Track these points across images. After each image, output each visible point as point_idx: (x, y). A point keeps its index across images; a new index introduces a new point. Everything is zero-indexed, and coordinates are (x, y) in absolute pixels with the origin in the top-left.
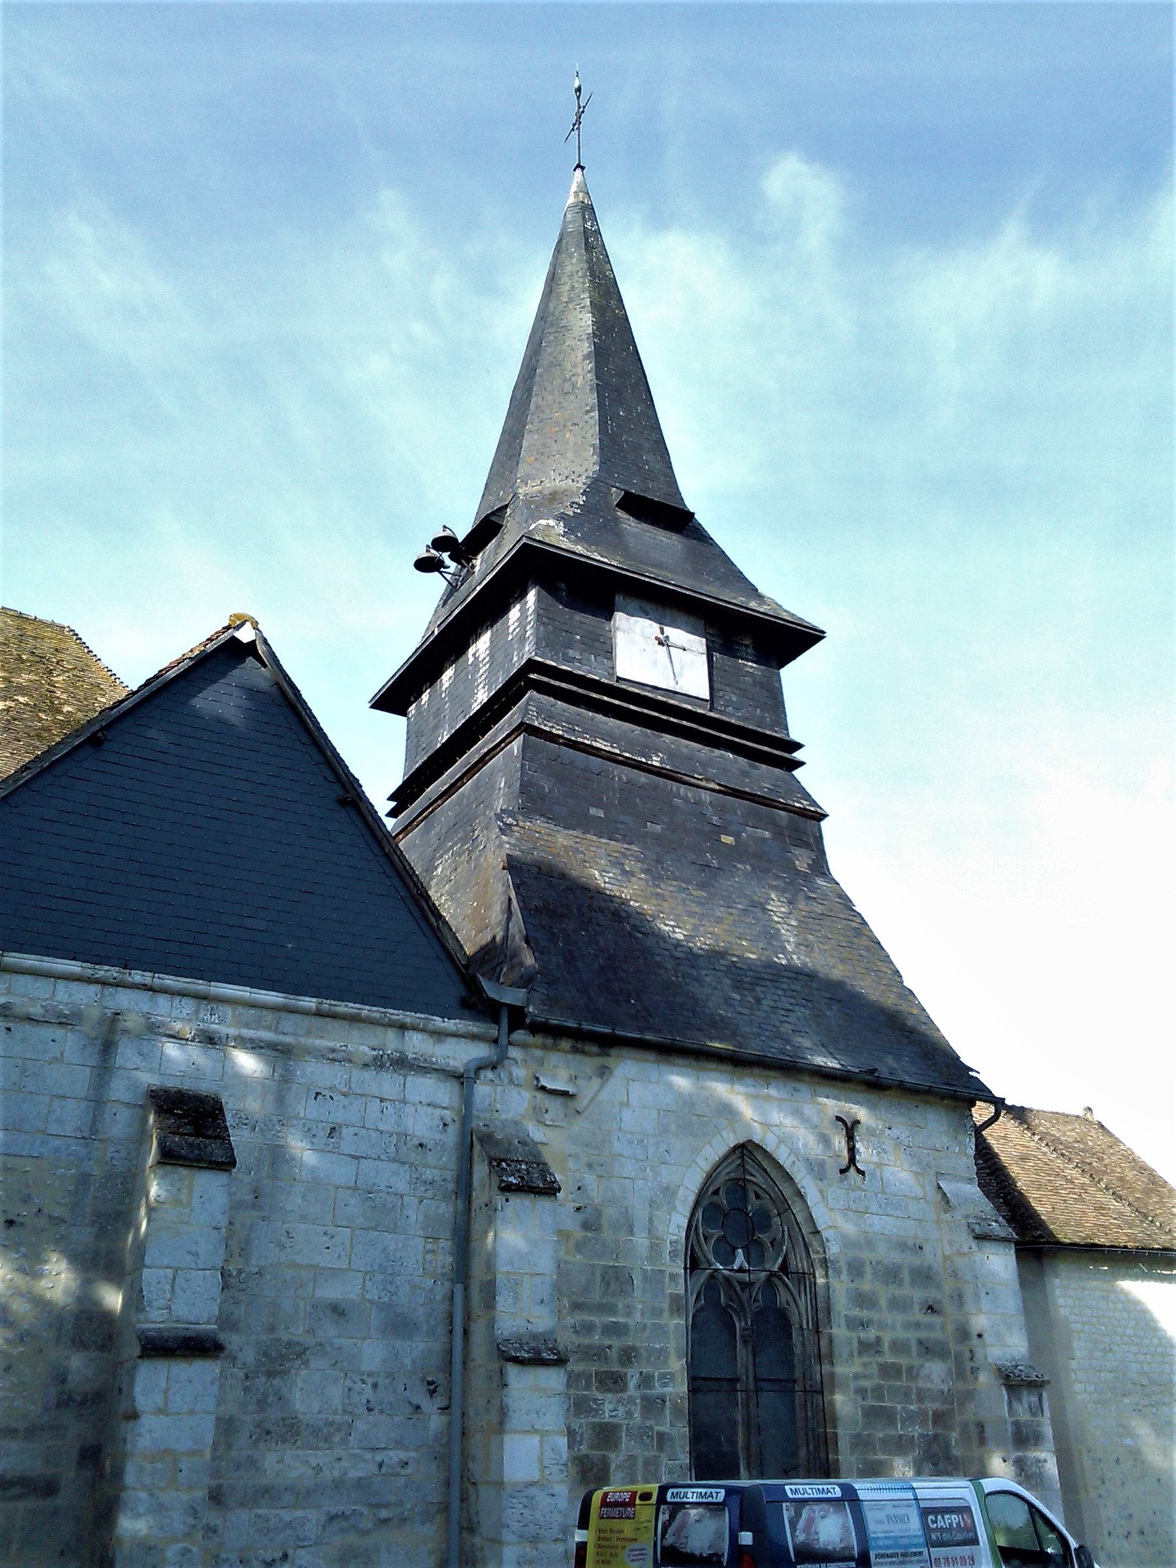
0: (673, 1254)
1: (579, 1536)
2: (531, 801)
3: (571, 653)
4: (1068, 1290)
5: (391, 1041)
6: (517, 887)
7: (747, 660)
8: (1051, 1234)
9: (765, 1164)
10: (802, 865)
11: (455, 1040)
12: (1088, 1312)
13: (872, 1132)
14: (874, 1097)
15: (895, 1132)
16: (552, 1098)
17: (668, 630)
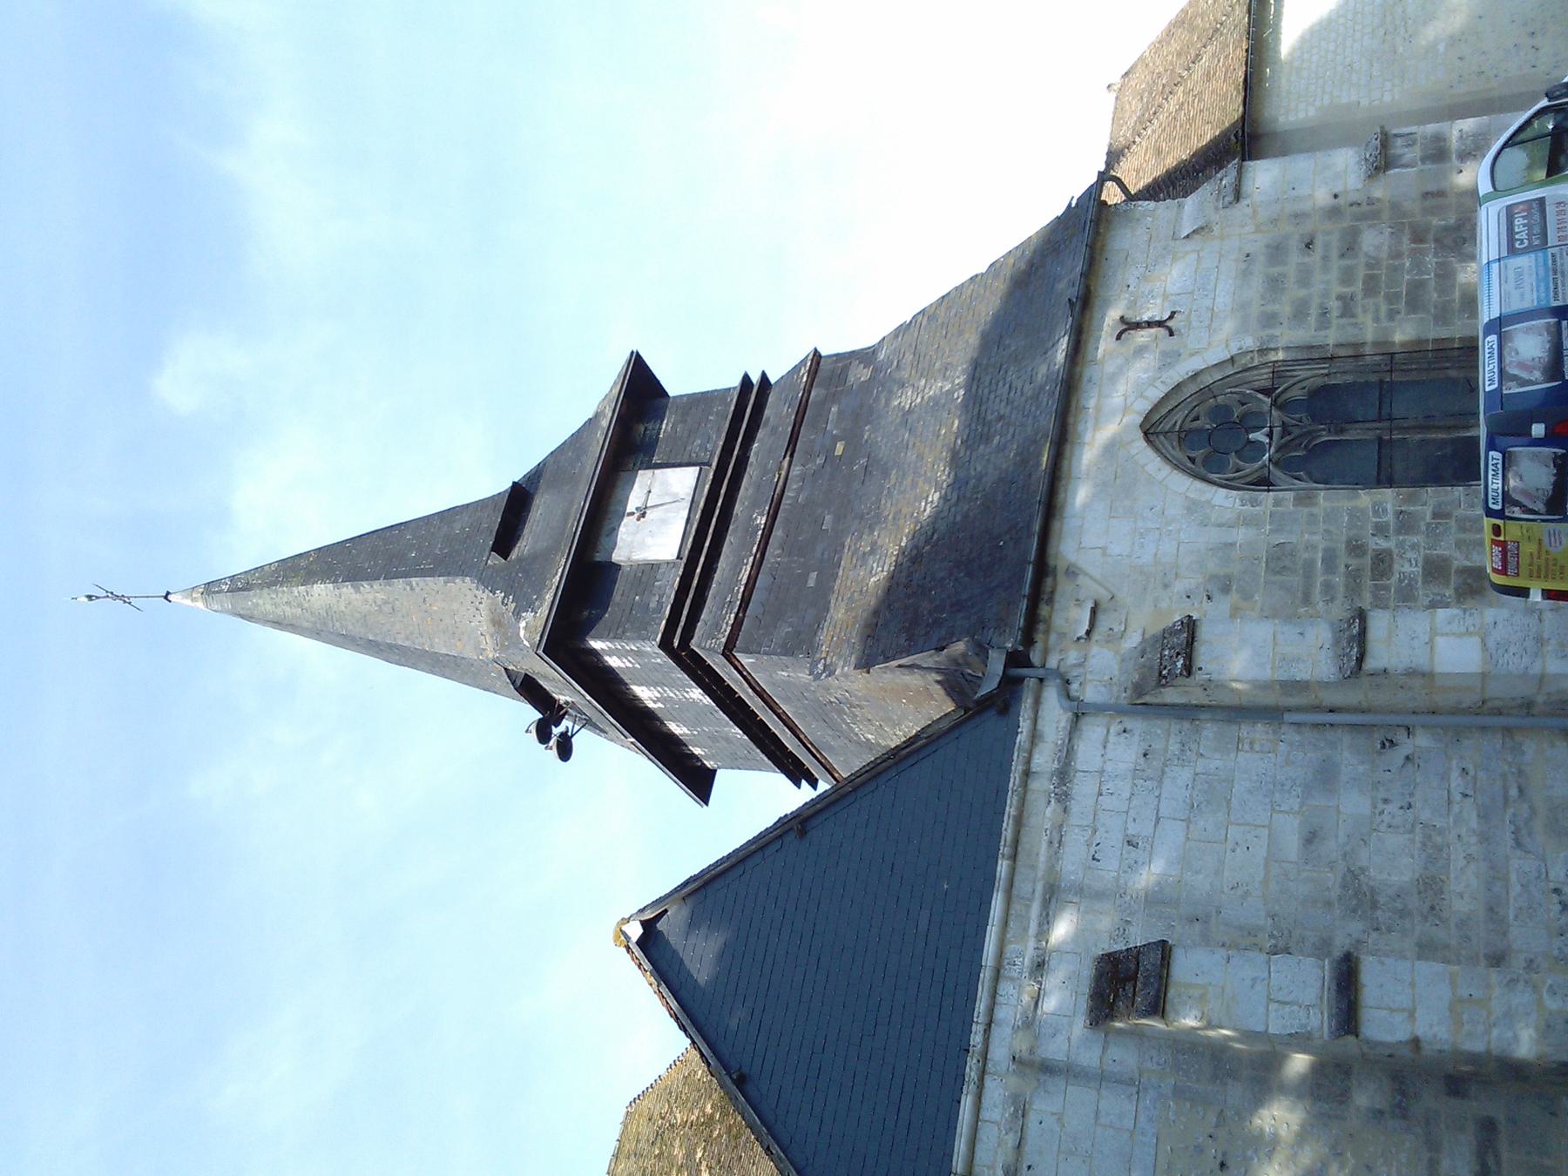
0: (1254, 503)
1: (1536, 596)
2: (801, 644)
3: (653, 605)
4: (1290, 106)
5: (1041, 785)
6: (887, 659)
8: (1234, 125)
9: (1164, 411)
11: (1040, 721)
13: (1132, 304)
14: (1097, 303)
15: (1132, 281)
17: (630, 508)
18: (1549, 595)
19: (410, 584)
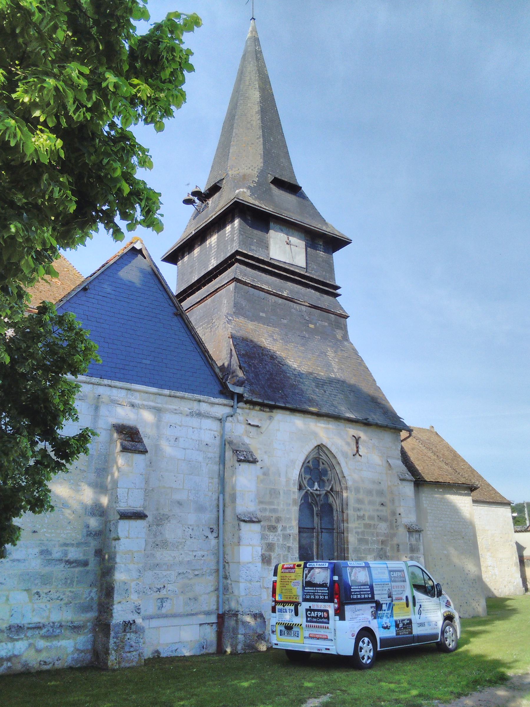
0: (294, 484)
1: (275, 578)
2: (238, 310)
3: (253, 247)
4: (430, 498)
5: (195, 406)
6: (235, 346)
8: (423, 477)
9: (326, 452)
10: (339, 337)
11: (218, 406)
12: (434, 506)
13: (364, 441)
14: (366, 428)
16: (252, 428)
17: (291, 238)
19: (259, 138)
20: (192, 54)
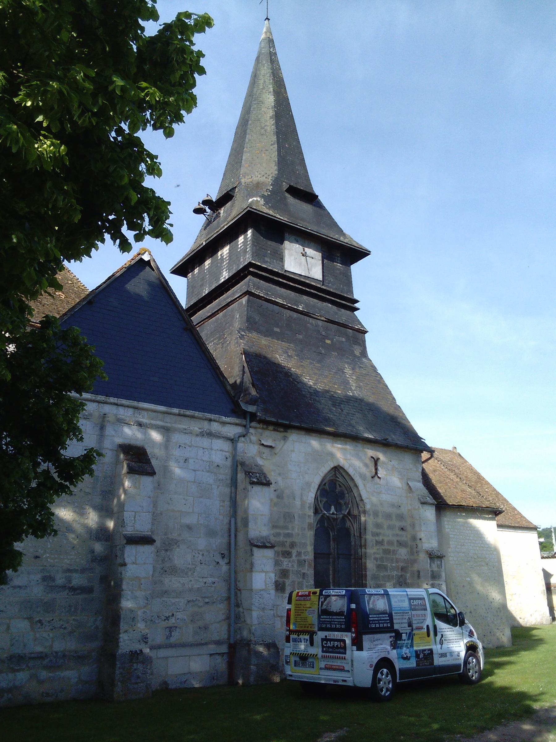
0: (309, 508)
1: (289, 607)
2: (251, 325)
3: (266, 259)
4: (451, 522)
5: (206, 425)
7: (338, 263)
9: (343, 474)
10: (357, 353)
13: (384, 463)
14: (385, 449)
15: (393, 463)
18: (289, 611)
19: (274, 144)
20: (203, 56)
